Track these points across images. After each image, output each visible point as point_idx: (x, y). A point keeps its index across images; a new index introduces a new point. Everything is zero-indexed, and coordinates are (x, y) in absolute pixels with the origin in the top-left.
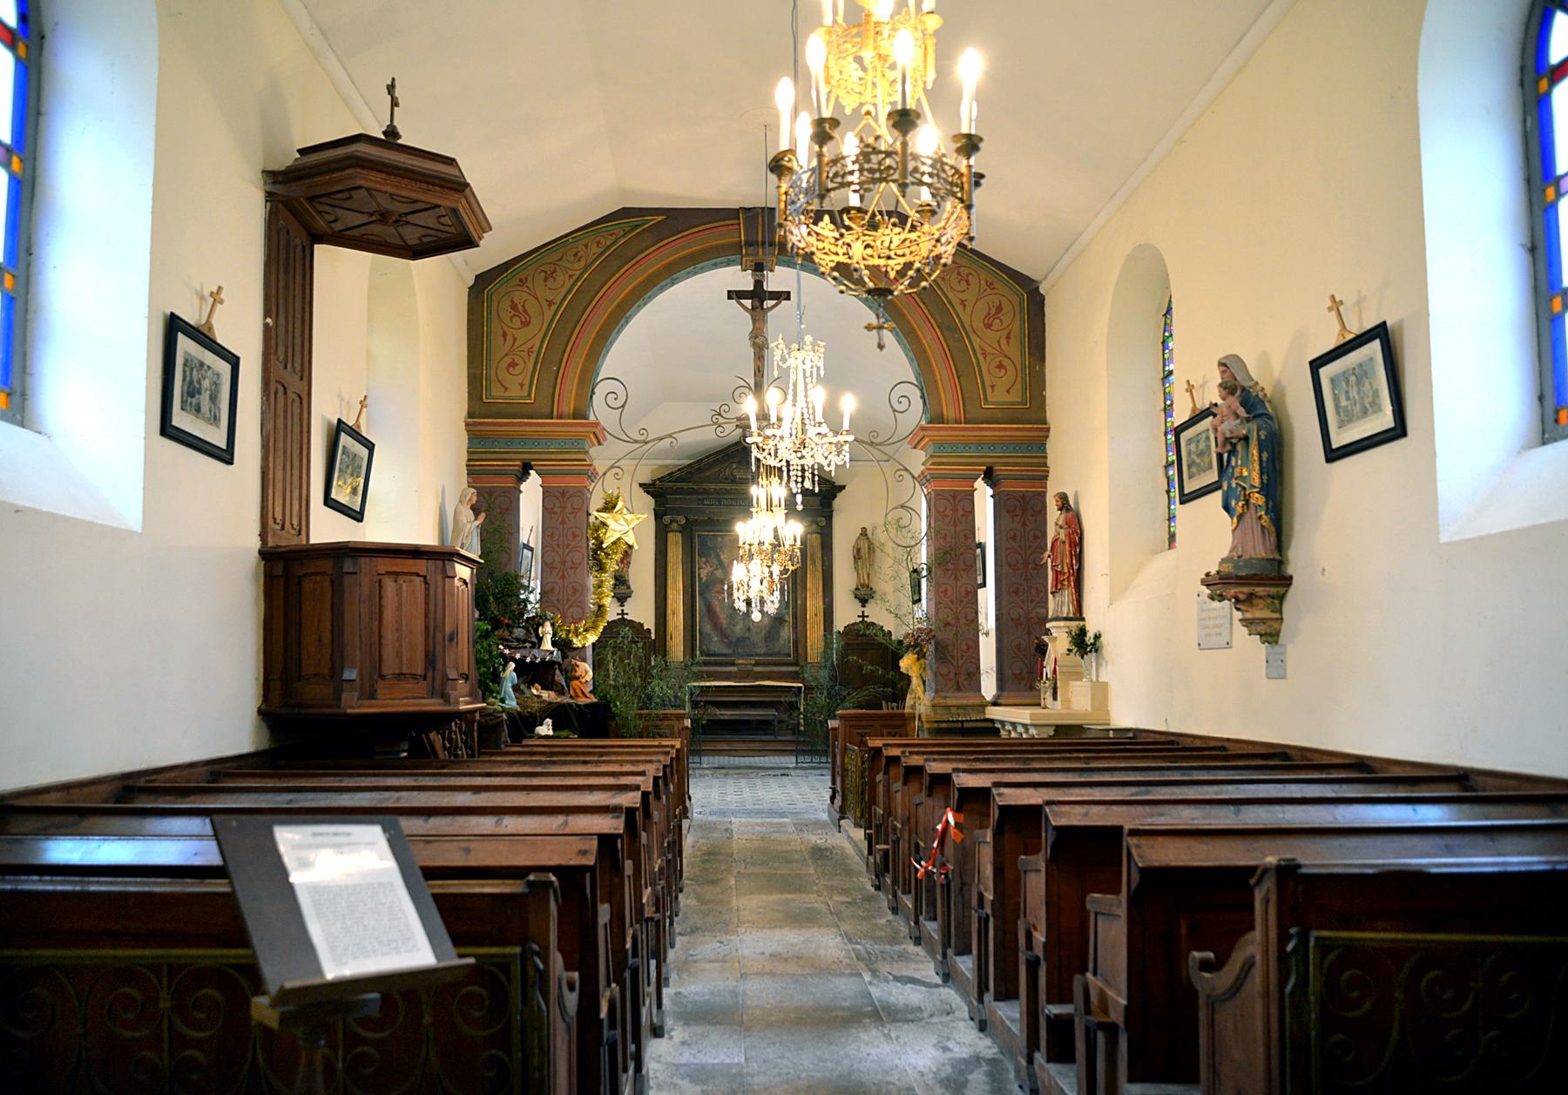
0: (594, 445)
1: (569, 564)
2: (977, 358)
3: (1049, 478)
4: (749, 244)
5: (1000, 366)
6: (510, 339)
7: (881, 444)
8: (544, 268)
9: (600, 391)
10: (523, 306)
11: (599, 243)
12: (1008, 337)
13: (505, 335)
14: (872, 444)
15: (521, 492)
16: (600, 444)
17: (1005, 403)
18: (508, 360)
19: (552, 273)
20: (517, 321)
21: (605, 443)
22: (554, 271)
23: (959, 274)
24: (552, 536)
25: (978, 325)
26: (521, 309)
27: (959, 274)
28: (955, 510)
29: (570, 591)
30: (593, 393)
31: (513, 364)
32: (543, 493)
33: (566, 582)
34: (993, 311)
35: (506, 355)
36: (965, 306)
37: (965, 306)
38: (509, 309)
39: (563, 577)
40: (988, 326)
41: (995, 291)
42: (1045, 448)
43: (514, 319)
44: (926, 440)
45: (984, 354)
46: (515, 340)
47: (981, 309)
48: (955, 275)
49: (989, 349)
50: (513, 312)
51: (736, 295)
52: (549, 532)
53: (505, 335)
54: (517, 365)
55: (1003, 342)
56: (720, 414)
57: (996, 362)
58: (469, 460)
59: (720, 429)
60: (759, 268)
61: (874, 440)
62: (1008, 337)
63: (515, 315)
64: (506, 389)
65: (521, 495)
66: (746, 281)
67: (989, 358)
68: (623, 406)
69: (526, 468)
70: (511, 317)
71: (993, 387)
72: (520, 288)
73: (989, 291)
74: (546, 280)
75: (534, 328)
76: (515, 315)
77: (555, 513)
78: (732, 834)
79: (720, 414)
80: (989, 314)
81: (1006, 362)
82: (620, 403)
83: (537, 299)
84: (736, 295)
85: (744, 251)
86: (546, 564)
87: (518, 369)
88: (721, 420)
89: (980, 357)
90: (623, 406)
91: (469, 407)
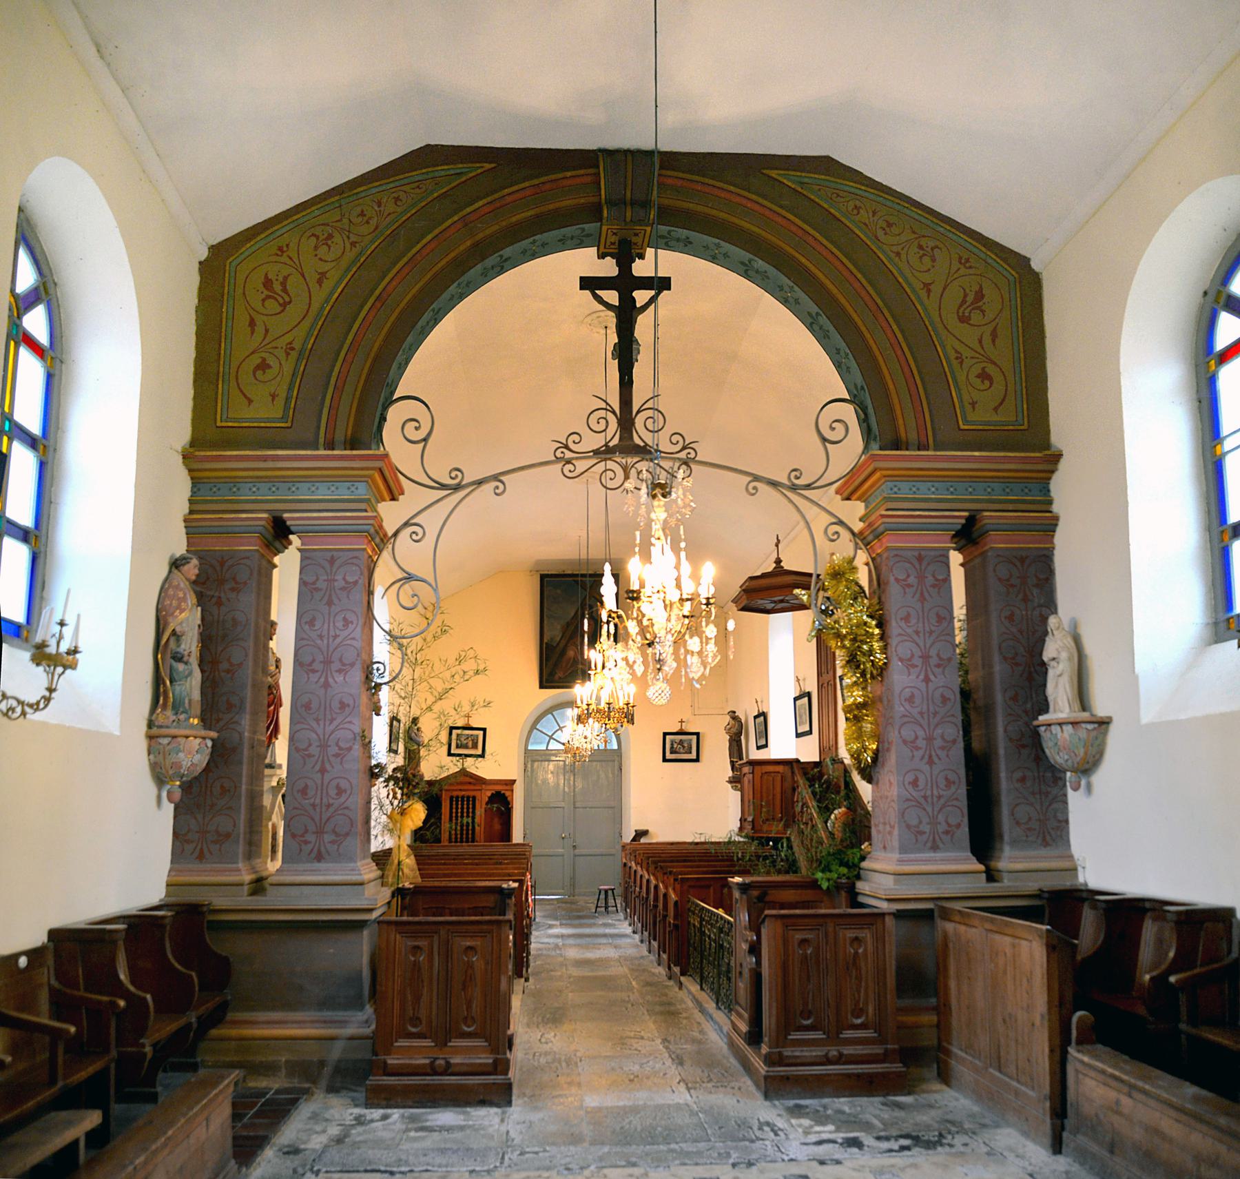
0: (384, 500)
1: (333, 750)
2: (950, 365)
3: (1059, 529)
4: (617, 203)
5: (984, 376)
6: (260, 329)
7: (808, 487)
8: (318, 231)
9: (395, 415)
10: (284, 284)
11: (397, 199)
12: (994, 335)
13: (252, 323)
14: (794, 488)
15: (275, 566)
16: (393, 499)
17: (988, 423)
18: (256, 360)
19: (327, 239)
20: (272, 306)
21: (401, 497)
22: (330, 236)
23: (921, 247)
24: (311, 623)
25: (952, 320)
26: (277, 287)
27: (921, 247)
28: (921, 578)
29: (333, 792)
30: (383, 419)
31: (263, 366)
32: (302, 560)
33: (327, 777)
34: (970, 299)
35: (253, 353)
36: (929, 291)
37: (929, 291)
38: (262, 289)
39: (323, 771)
40: (964, 319)
41: (971, 271)
42: (1049, 491)
43: (267, 303)
44: (877, 475)
45: (960, 358)
46: (267, 331)
47: (954, 295)
48: (914, 249)
49: (966, 353)
50: (266, 293)
51: (588, 284)
52: (305, 619)
53: (252, 323)
54: (269, 367)
55: (987, 340)
56: (566, 447)
57: (977, 370)
58: (191, 512)
59: (570, 467)
60: (625, 254)
61: (797, 482)
62: (994, 335)
63: (268, 297)
64: (250, 401)
65: (275, 571)
66: (609, 268)
67: (967, 363)
68: (425, 440)
69: (279, 532)
70: (263, 300)
71: (973, 404)
72: (277, 259)
73: (963, 271)
74: (316, 248)
75: (294, 311)
76: (268, 297)
77: (314, 671)
78: (644, 655)
79: (566, 447)
80: (964, 301)
81: (991, 369)
82: (421, 434)
83: (303, 275)
84: (588, 284)
85: (605, 214)
86: (297, 750)
87: (270, 373)
88: (568, 455)
89: (955, 363)
90: (425, 440)
91: (193, 431)
